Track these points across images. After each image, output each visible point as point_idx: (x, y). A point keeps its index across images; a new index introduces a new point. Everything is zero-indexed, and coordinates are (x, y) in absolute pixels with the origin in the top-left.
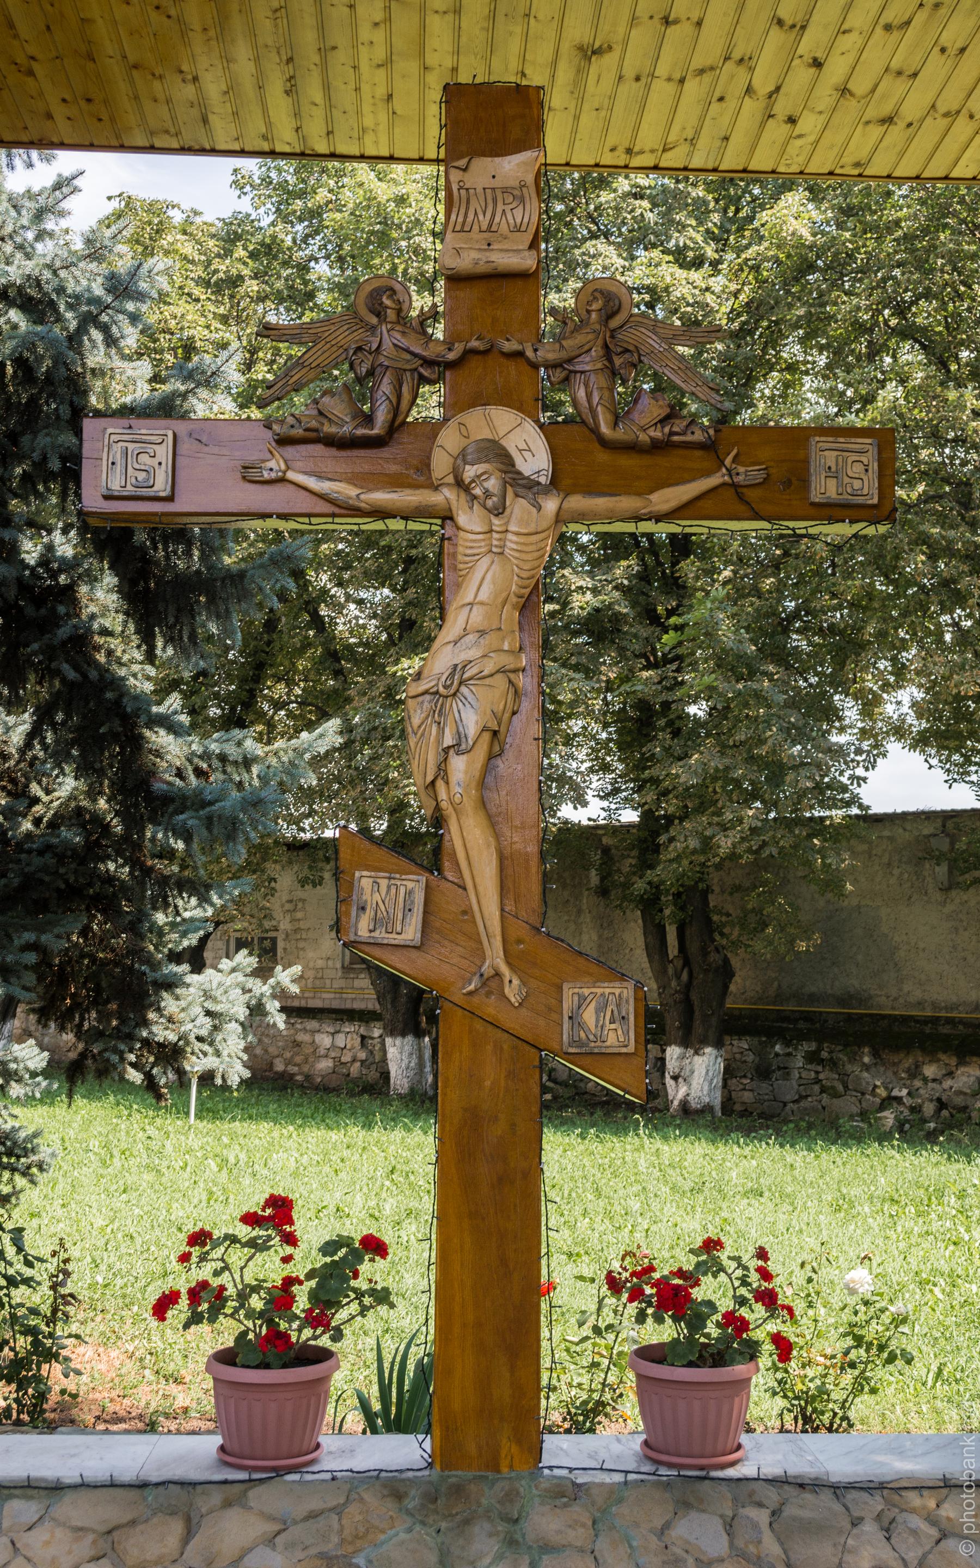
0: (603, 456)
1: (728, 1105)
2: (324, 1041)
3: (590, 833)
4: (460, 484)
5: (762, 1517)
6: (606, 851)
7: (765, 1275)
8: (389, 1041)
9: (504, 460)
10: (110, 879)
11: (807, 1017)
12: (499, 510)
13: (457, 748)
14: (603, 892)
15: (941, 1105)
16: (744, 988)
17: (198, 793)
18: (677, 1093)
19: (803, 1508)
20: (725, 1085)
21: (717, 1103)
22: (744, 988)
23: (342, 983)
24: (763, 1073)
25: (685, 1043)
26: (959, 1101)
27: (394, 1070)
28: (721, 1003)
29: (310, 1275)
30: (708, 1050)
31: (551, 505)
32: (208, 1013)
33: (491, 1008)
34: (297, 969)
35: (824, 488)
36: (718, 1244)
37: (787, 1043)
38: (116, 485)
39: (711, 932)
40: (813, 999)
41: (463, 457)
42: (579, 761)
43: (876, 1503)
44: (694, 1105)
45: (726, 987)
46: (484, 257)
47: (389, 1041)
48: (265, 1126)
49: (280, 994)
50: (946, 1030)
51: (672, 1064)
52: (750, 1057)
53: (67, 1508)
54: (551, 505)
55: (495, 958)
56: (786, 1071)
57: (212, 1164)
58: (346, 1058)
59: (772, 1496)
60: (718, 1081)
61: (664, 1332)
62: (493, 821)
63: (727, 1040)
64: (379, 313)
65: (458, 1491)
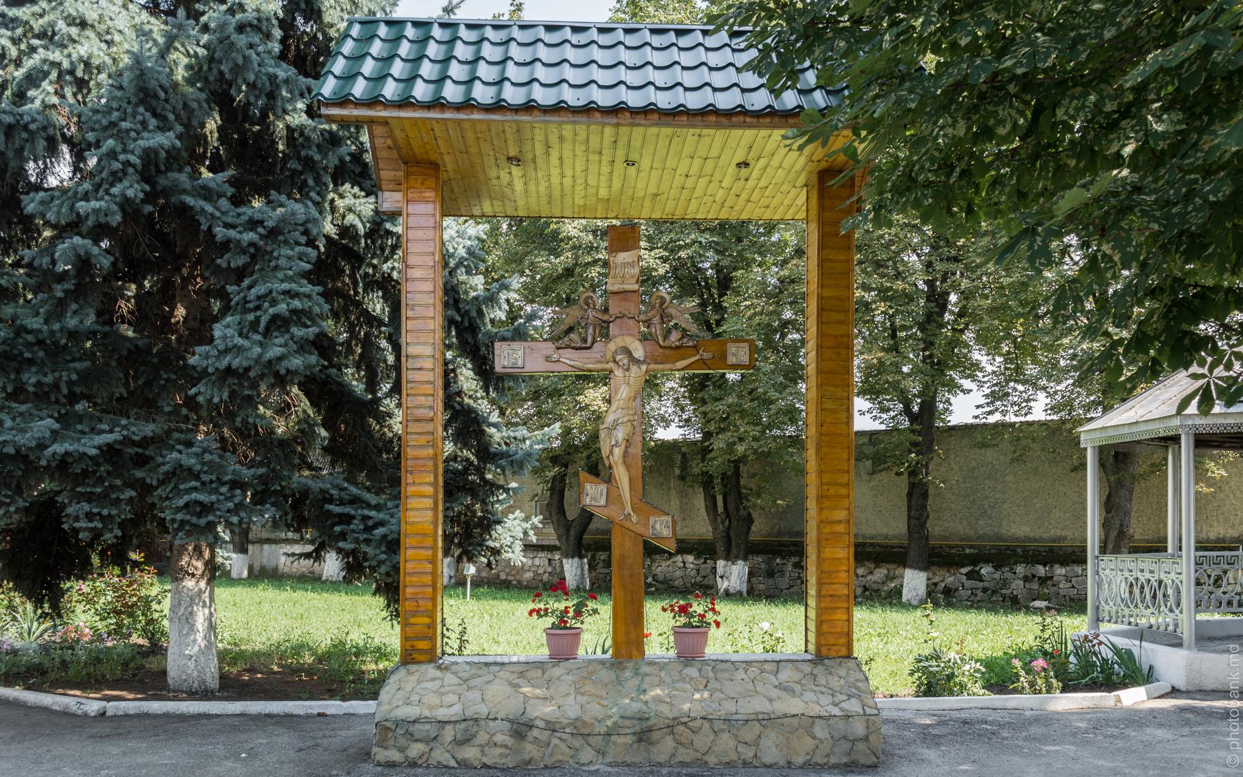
1: (751, 592)
3: (674, 446)
6: (684, 455)
8: (565, 561)
9: (628, 352)
10: (473, 482)
12: (628, 370)
13: (616, 445)
15: (865, 589)
16: (760, 529)
17: (507, 452)
18: (723, 585)
19: (719, 666)
20: (749, 581)
21: (745, 590)
22: (760, 529)
24: (770, 574)
25: (727, 558)
26: (875, 586)
31: (644, 367)
33: (628, 524)
35: (731, 360)
37: (783, 558)
39: (741, 499)
42: (667, 408)
44: (732, 591)
47: (565, 561)
48: (505, 603)
49: (534, 528)
50: (869, 549)
51: (720, 571)
52: (763, 566)
53: (507, 667)
54: (644, 367)
55: (629, 509)
56: (782, 573)
58: (540, 571)
63: (750, 557)
64: (588, 305)
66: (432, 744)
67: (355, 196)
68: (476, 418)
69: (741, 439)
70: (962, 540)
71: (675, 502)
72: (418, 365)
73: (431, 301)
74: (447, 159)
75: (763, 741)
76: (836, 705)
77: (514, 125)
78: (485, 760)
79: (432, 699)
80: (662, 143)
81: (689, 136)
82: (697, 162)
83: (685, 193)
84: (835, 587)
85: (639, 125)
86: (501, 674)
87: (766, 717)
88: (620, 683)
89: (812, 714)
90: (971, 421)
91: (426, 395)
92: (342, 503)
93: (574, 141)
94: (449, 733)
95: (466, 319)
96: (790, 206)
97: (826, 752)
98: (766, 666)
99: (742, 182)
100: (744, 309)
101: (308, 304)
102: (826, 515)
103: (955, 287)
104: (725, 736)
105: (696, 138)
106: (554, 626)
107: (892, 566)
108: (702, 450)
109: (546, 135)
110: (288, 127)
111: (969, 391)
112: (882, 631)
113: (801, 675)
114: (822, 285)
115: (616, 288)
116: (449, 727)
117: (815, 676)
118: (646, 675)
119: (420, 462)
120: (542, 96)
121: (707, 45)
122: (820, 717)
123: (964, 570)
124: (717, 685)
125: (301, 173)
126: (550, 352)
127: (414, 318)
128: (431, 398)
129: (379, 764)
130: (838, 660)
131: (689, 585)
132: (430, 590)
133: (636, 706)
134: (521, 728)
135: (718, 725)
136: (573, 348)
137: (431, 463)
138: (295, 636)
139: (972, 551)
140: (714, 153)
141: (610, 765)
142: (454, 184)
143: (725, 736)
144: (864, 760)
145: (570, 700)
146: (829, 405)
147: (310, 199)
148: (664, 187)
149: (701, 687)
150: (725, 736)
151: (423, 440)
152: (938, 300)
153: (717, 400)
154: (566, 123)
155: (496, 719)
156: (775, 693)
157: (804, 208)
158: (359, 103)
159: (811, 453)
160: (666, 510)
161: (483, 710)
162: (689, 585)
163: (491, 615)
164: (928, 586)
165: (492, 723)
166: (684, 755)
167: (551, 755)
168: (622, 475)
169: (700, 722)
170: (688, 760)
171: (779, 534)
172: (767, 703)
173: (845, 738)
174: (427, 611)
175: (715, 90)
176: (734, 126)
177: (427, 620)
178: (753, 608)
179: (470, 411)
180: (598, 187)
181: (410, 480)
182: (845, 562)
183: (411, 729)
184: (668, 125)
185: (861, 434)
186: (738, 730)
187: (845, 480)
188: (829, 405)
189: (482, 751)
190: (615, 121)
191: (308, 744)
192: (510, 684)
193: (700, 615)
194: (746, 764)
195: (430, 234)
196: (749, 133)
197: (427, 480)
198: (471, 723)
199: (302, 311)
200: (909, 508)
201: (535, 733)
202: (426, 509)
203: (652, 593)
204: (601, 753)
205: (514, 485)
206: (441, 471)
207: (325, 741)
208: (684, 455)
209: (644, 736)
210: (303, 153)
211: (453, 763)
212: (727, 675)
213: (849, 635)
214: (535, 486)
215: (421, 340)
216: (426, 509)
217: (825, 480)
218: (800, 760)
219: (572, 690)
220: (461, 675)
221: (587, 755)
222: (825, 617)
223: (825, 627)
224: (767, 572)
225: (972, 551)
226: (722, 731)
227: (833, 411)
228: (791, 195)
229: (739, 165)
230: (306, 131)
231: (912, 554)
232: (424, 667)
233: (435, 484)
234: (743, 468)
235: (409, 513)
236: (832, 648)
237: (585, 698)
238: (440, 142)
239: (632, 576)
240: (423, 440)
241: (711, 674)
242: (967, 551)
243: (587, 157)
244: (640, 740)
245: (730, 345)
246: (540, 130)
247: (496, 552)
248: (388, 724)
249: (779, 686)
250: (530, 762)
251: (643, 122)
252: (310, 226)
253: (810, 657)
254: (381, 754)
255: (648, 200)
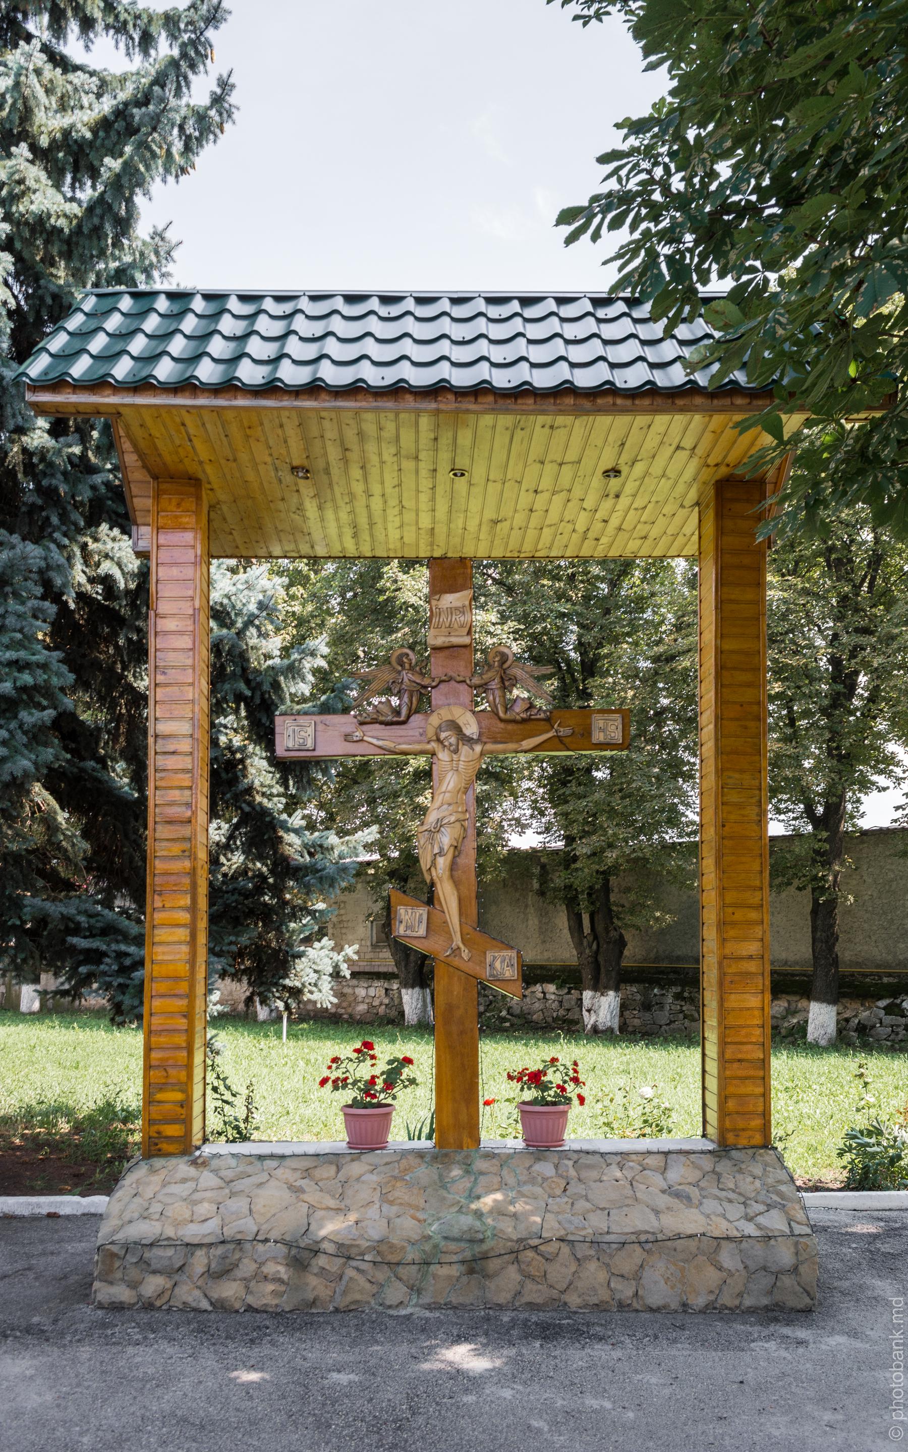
0: (502, 725)
1: (623, 1027)
2: (361, 992)
3: (533, 855)
4: (438, 740)
5: (570, 1163)
6: (543, 867)
7: (575, 1071)
8: (403, 991)
10: (265, 904)
11: (675, 971)
12: (456, 751)
13: (441, 853)
14: (542, 893)
16: (634, 952)
18: (589, 1020)
19: (585, 1160)
20: (622, 1015)
21: (616, 1026)
22: (634, 952)
23: (371, 955)
24: (647, 1006)
25: (595, 988)
27: (407, 1009)
28: (618, 963)
29: (383, 1073)
30: (611, 993)
31: (478, 748)
32: (316, 971)
33: (456, 962)
34: (356, 947)
35: (598, 737)
36: (557, 1060)
37: (662, 988)
38: (290, 745)
40: (679, 959)
41: (440, 728)
42: (524, 811)
43: (619, 1158)
44: (601, 1027)
45: (621, 953)
46: (447, 639)
47: (403, 991)
49: (348, 960)
51: (587, 1003)
52: (638, 997)
53: (288, 1163)
54: (478, 748)
55: (457, 941)
56: (661, 1005)
57: (302, 1063)
58: (376, 1003)
59: (575, 1156)
60: (617, 1011)
61: (529, 1095)
62: (456, 883)
63: (622, 986)
64: (402, 664)
65: (446, 1155)
66: (176, 1277)
67: (114, 539)
68: (271, 822)
69: (611, 846)
70: (878, 966)
71: (533, 922)
72: (171, 748)
73: (189, 662)
74: (209, 469)
75: (647, 1274)
76: (750, 1219)
77: (294, 414)
78: (250, 1300)
79: (180, 1210)
80: (502, 439)
81: (538, 428)
82: (550, 469)
83: (534, 522)
84: (745, 1048)
85: (467, 411)
86: (279, 1172)
87: (651, 1238)
88: (444, 1187)
89: (717, 1234)
90: (886, 824)
91: (181, 788)
92: (91, 934)
93: (379, 439)
94: (199, 1262)
95: (258, 693)
96: (675, 536)
97: (737, 1291)
98: (650, 1161)
99: (610, 502)
100: (615, 687)
101: (42, 677)
102: (731, 948)
103: (866, 665)
104: (592, 1266)
105: (547, 430)
106: (355, 1104)
107: (793, 998)
108: (567, 859)
109: (340, 431)
110: (25, 450)
111: (885, 789)
112: (790, 1084)
113: (698, 1174)
114: (721, 635)
115: (440, 641)
116: (200, 1253)
117: (719, 1176)
118: (482, 1173)
119: (173, 878)
120: (330, 374)
121: (562, 315)
122: (728, 1238)
123: (882, 1003)
124: (580, 1189)
125: (42, 508)
126: (348, 729)
127: (167, 685)
128: (187, 793)
129: (101, 1306)
130: (750, 1152)
131: (550, 1020)
132: (185, 1054)
133: (466, 1221)
134: (301, 1254)
135: (583, 1250)
136: (382, 723)
137: (187, 881)
138: (51, 1097)
139: (891, 980)
140: (571, 456)
141: (429, 1307)
142: (225, 508)
143: (592, 1266)
144: (792, 1302)
145: (373, 1212)
146: (733, 797)
147: (55, 541)
148: (506, 511)
149: (558, 1192)
150: (592, 1266)
151: (176, 849)
152: (844, 680)
153: (580, 797)
154: (367, 410)
155: (266, 1240)
156: (663, 1201)
157: (695, 538)
158: (79, 386)
159: (709, 864)
160: (512, 943)
161: (249, 1226)
162: (550, 1020)
163: (308, 1062)
164: (838, 1022)
165: (261, 1247)
166: (534, 1293)
167: (345, 1293)
168: (447, 893)
169: (557, 1245)
170: (540, 1301)
171: (657, 959)
172: (652, 1216)
173: (764, 1268)
174: (180, 1083)
175: (568, 342)
176: (600, 411)
177: (179, 1096)
178: (627, 1051)
179: (264, 812)
180: (417, 512)
181: (158, 904)
182: (757, 1013)
183: (147, 1255)
184: (507, 411)
185: (773, 839)
186: (611, 1256)
187: (756, 900)
188: (733, 797)
189: (247, 1287)
190: (433, 405)
191: (18, 1266)
192: (291, 1187)
193: (558, 1086)
194: (622, 1306)
195: (189, 572)
196: (622, 421)
197: (182, 903)
198: (231, 1246)
199: (36, 687)
200: (814, 930)
201: (322, 1261)
202: (180, 943)
203: (506, 1030)
204: (416, 1289)
205: (321, 906)
206: (203, 890)
207: (43, 1260)
208: (543, 867)
209: (476, 1266)
210: (45, 483)
211: (205, 1305)
212: (594, 1174)
213: (766, 1115)
214: (370, 903)
215: (176, 713)
216: (180, 943)
217: (728, 900)
218: (700, 1301)
219: (376, 1197)
220: (223, 1173)
221: (395, 1293)
222: (731, 1090)
223: (731, 1105)
224: (643, 1004)
225: (891, 980)
226: (588, 1258)
227: (740, 806)
228: (677, 520)
229: (607, 473)
230: (49, 455)
231: (819, 984)
232: (173, 1161)
233: (193, 909)
234: (613, 880)
235: (158, 949)
236: (741, 1129)
237: (394, 1209)
238: (197, 443)
239: (462, 1033)
240: (176, 849)
241: (572, 1173)
242: (885, 980)
243: (399, 465)
244: (471, 1272)
245: (596, 717)
246: (331, 420)
247: (296, 993)
248: (115, 1249)
249: (668, 1191)
250: (314, 1303)
251: (472, 407)
252: (52, 574)
253: (711, 1146)
254: (104, 1292)
255: (485, 528)
